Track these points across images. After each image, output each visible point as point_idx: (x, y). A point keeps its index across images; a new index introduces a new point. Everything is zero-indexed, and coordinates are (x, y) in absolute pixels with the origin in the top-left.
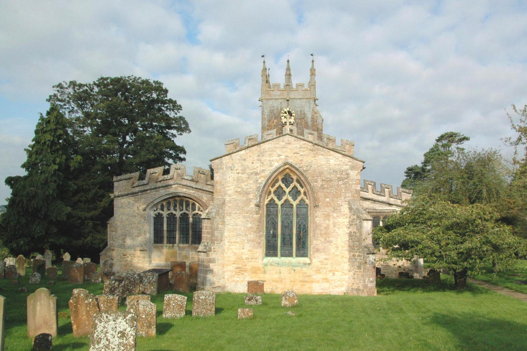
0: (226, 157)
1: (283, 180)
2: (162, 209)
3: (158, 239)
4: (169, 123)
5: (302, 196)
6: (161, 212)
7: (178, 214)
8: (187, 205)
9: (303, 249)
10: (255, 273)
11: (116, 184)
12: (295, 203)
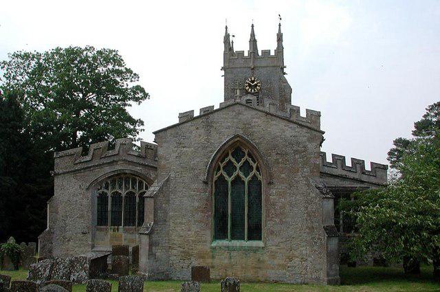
2: (107, 188)
3: (101, 220)
4: (125, 95)
5: (254, 171)
6: (105, 191)
7: (123, 193)
8: (134, 183)
9: (255, 233)
10: (202, 257)
11: (57, 161)
12: (246, 180)
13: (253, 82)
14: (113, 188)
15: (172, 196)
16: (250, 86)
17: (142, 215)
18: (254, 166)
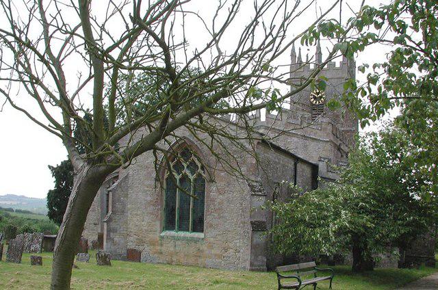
9: (198, 226)
10: (154, 245)
12: (192, 178)
13: (318, 94)
15: (130, 191)
16: (315, 98)
17: (200, 214)
18: (199, 165)
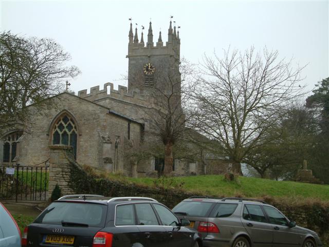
0: (155, 216)
1: (63, 120)
2: (9, 140)
5: (74, 129)
6: (8, 142)
12: (69, 133)
14: (13, 140)
